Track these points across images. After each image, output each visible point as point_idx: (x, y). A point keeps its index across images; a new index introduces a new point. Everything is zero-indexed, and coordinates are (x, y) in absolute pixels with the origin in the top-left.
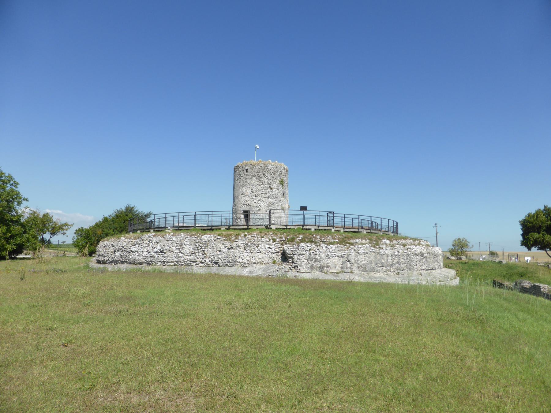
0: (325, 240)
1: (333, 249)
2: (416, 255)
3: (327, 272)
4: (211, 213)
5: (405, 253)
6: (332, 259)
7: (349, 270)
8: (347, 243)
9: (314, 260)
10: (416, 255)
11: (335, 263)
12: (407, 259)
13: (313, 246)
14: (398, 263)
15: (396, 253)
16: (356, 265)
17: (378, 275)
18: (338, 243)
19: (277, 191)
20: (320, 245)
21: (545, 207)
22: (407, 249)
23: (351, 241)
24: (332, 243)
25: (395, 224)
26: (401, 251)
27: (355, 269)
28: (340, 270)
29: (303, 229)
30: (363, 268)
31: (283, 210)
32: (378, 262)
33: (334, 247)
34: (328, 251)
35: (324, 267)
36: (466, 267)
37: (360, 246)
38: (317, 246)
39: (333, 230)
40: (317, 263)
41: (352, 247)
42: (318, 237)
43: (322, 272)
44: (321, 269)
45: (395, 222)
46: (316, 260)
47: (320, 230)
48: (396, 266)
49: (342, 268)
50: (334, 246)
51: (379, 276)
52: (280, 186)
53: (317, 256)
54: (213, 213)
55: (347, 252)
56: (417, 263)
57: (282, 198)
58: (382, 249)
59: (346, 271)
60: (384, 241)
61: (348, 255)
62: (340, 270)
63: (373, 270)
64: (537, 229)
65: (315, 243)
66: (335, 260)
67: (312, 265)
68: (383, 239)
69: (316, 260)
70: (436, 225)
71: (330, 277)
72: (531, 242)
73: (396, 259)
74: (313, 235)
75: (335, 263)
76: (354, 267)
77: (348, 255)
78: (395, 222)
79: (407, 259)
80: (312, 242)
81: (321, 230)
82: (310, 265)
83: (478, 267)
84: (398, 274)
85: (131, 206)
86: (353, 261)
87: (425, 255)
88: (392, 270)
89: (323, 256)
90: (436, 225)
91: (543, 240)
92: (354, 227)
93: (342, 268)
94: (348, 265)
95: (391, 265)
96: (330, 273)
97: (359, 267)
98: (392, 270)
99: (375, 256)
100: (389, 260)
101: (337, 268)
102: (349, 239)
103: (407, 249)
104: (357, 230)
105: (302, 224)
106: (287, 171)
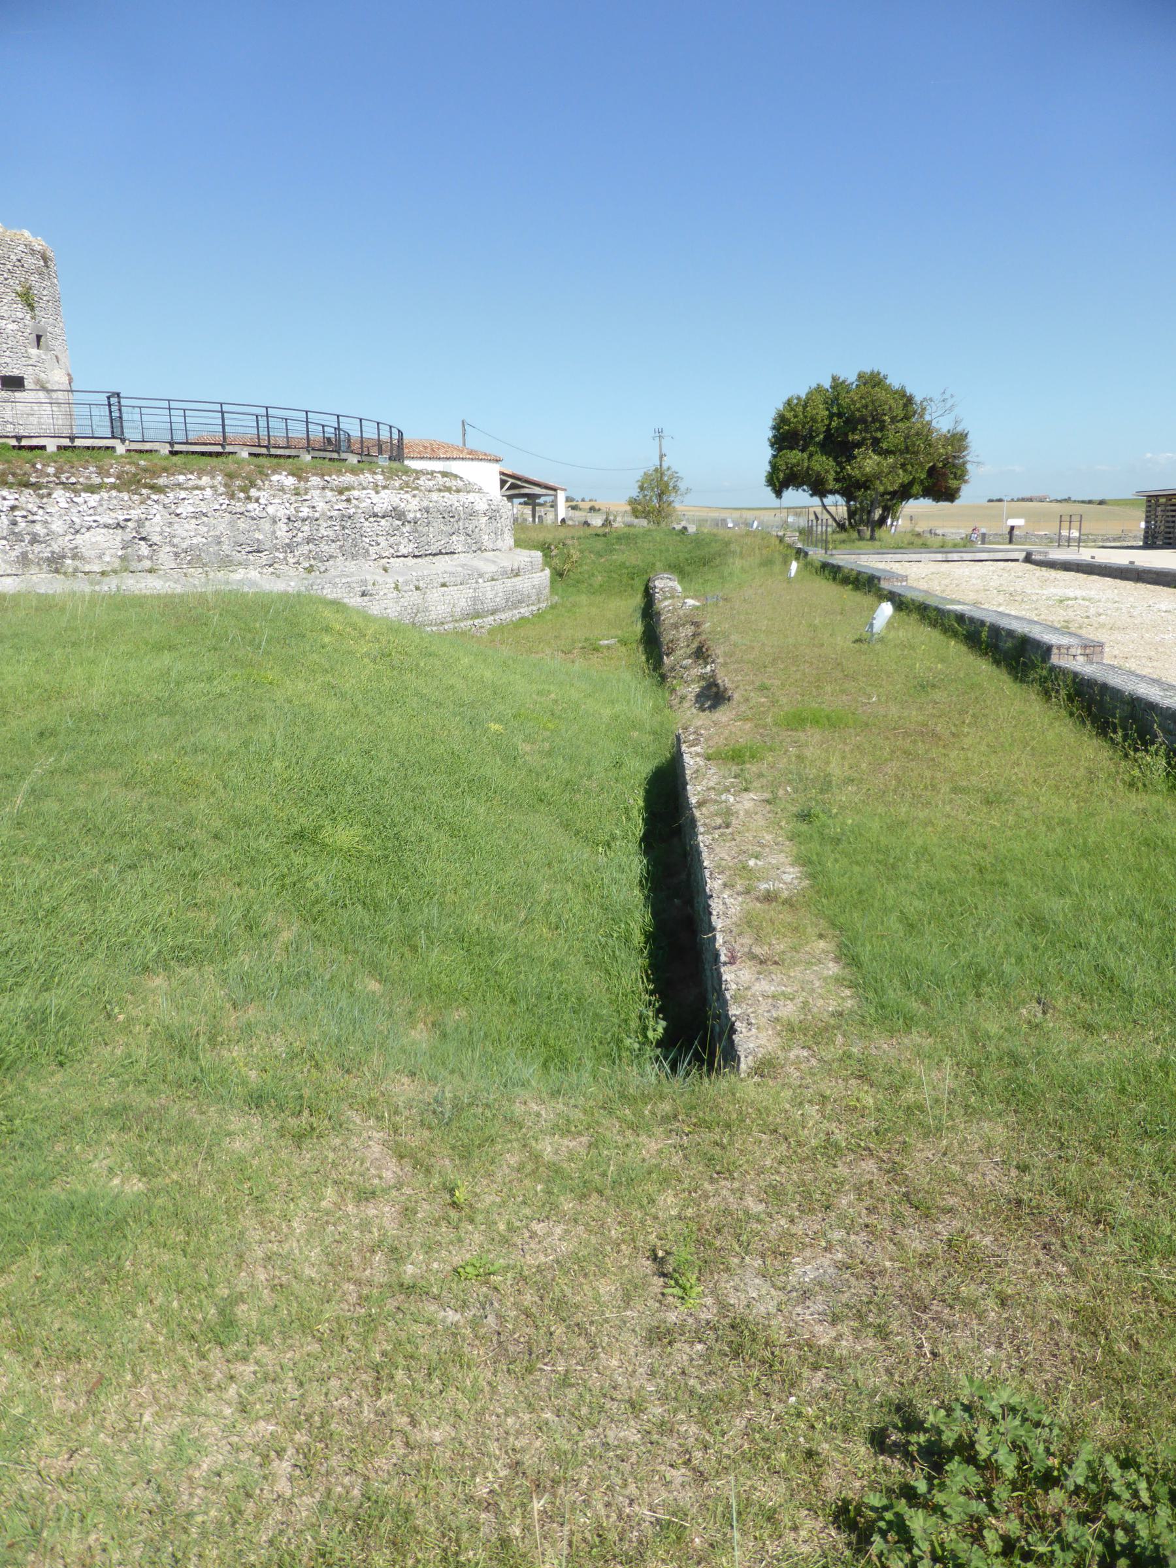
0: (73, 480)
1: (92, 503)
2: (376, 516)
3: (76, 570)
4: (166, 404)
5: (335, 513)
6: (88, 534)
7: (147, 564)
8: (146, 486)
9: (27, 538)
10: (376, 516)
11: (101, 545)
12: (344, 528)
13: (28, 499)
14: (309, 541)
15: (305, 512)
16: (168, 549)
17: (239, 575)
18: (113, 487)
19: (14, 326)
20: (50, 495)
21: (834, 379)
22: (348, 500)
23: (161, 481)
24: (92, 489)
25: (395, 436)
26: (321, 506)
27: (165, 558)
28: (117, 564)
29: (21, 448)
30: (192, 557)
31: (44, 389)
32: (242, 539)
33: (93, 499)
34: (74, 510)
35: (64, 557)
36: (599, 545)
37: (183, 494)
38: (42, 497)
39: (121, 449)
40: (37, 548)
41: (155, 497)
42: (51, 470)
43: (57, 571)
44: (55, 563)
45: (395, 431)
46: (35, 539)
47: (271, 456)
48: (304, 549)
49: (123, 559)
50: (96, 497)
51: (252, 578)
52: (20, 311)
53: (39, 529)
54: (173, 404)
55: (135, 514)
56: (380, 539)
57: (34, 351)
58: (257, 500)
59: (134, 565)
60: (275, 478)
61: (140, 523)
62: (117, 564)
63: (226, 563)
64: (804, 438)
65: (36, 486)
66: (99, 537)
67: (24, 555)
68: (274, 472)
69: (35, 539)
70: (659, 433)
71: (83, 586)
72: (782, 476)
73: (306, 528)
74: (34, 466)
75: (101, 545)
76: (161, 555)
77: (140, 523)
78: (395, 431)
79: (344, 528)
80: (27, 485)
81: (181, 452)
82: (14, 554)
83: (628, 545)
84: (310, 569)
85: (814, 386)
86: (156, 538)
87: (410, 516)
88: (291, 561)
89: (57, 526)
90: (659, 433)
91: (808, 468)
92: (293, 443)
93: (123, 559)
94: (144, 549)
95: (290, 547)
96: (86, 573)
97: (176, 555)
98: (291, 561)
99: (232, 524)
100: (279, 534)
101: (107, 559)
102: (155, 474)
103: (348, 500)
104: (219, 449)
105: (220, 439)
106: (45, 258)
